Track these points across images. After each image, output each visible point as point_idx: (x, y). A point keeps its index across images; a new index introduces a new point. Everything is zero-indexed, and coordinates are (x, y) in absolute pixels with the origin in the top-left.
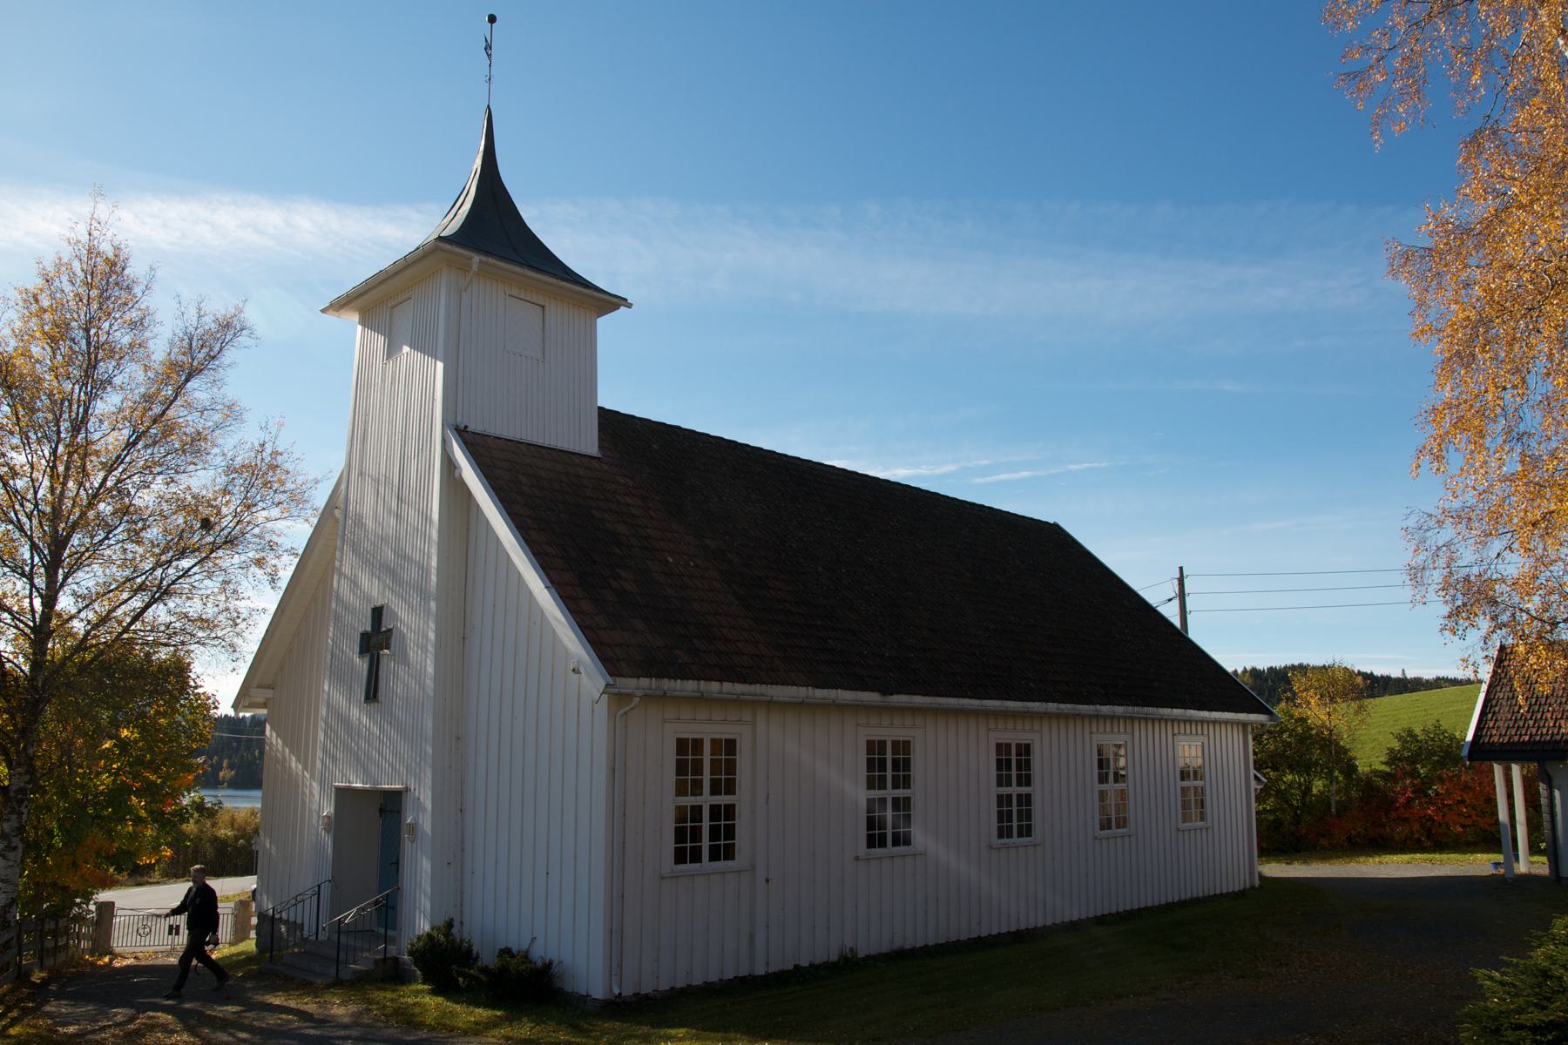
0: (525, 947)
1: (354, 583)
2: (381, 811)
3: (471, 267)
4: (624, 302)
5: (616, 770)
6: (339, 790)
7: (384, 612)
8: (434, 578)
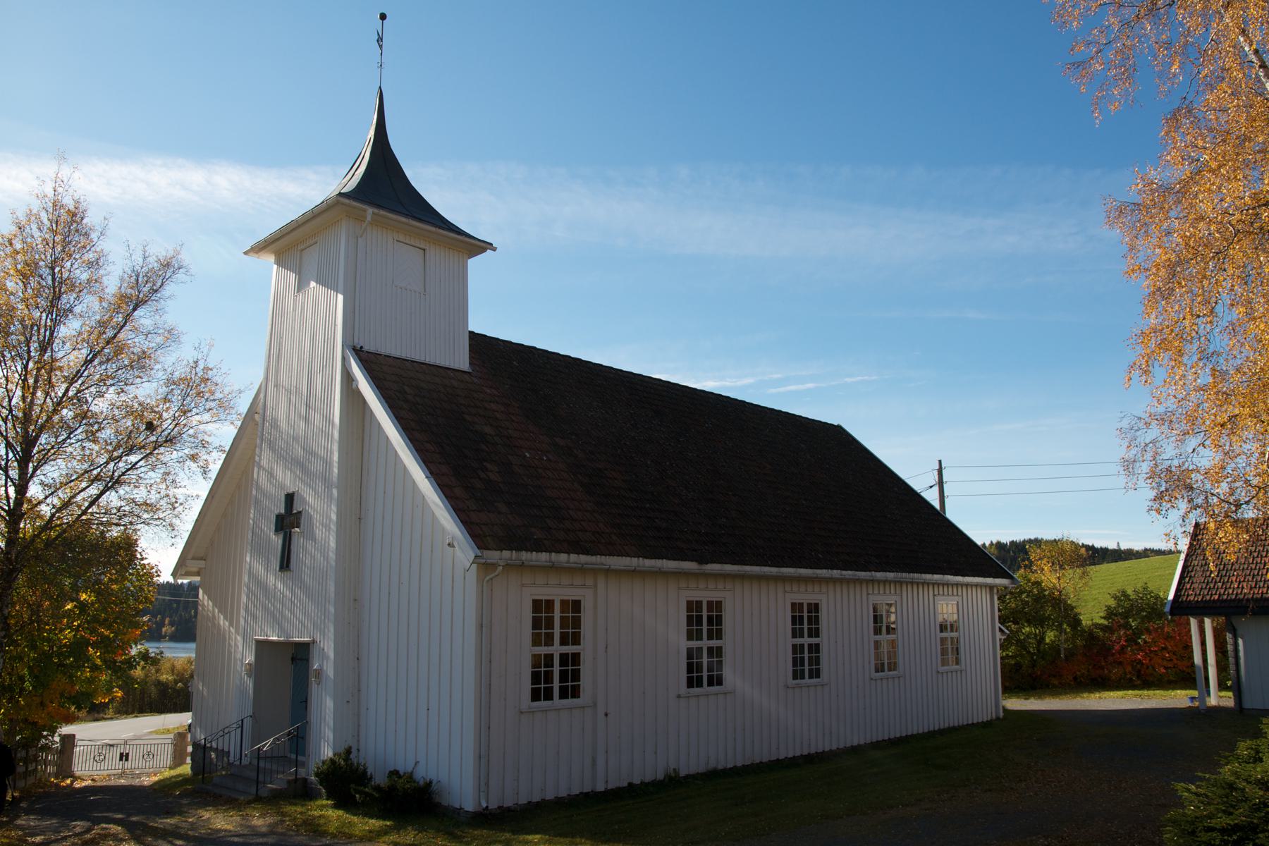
0: (410, 770)
1: (271, 475)
2: (293, 659)
3: (366, 218)
4: (489, 246)
5: (485, 626)
6: (258, 642)
7: (295, 498)
8: (336, 470)
